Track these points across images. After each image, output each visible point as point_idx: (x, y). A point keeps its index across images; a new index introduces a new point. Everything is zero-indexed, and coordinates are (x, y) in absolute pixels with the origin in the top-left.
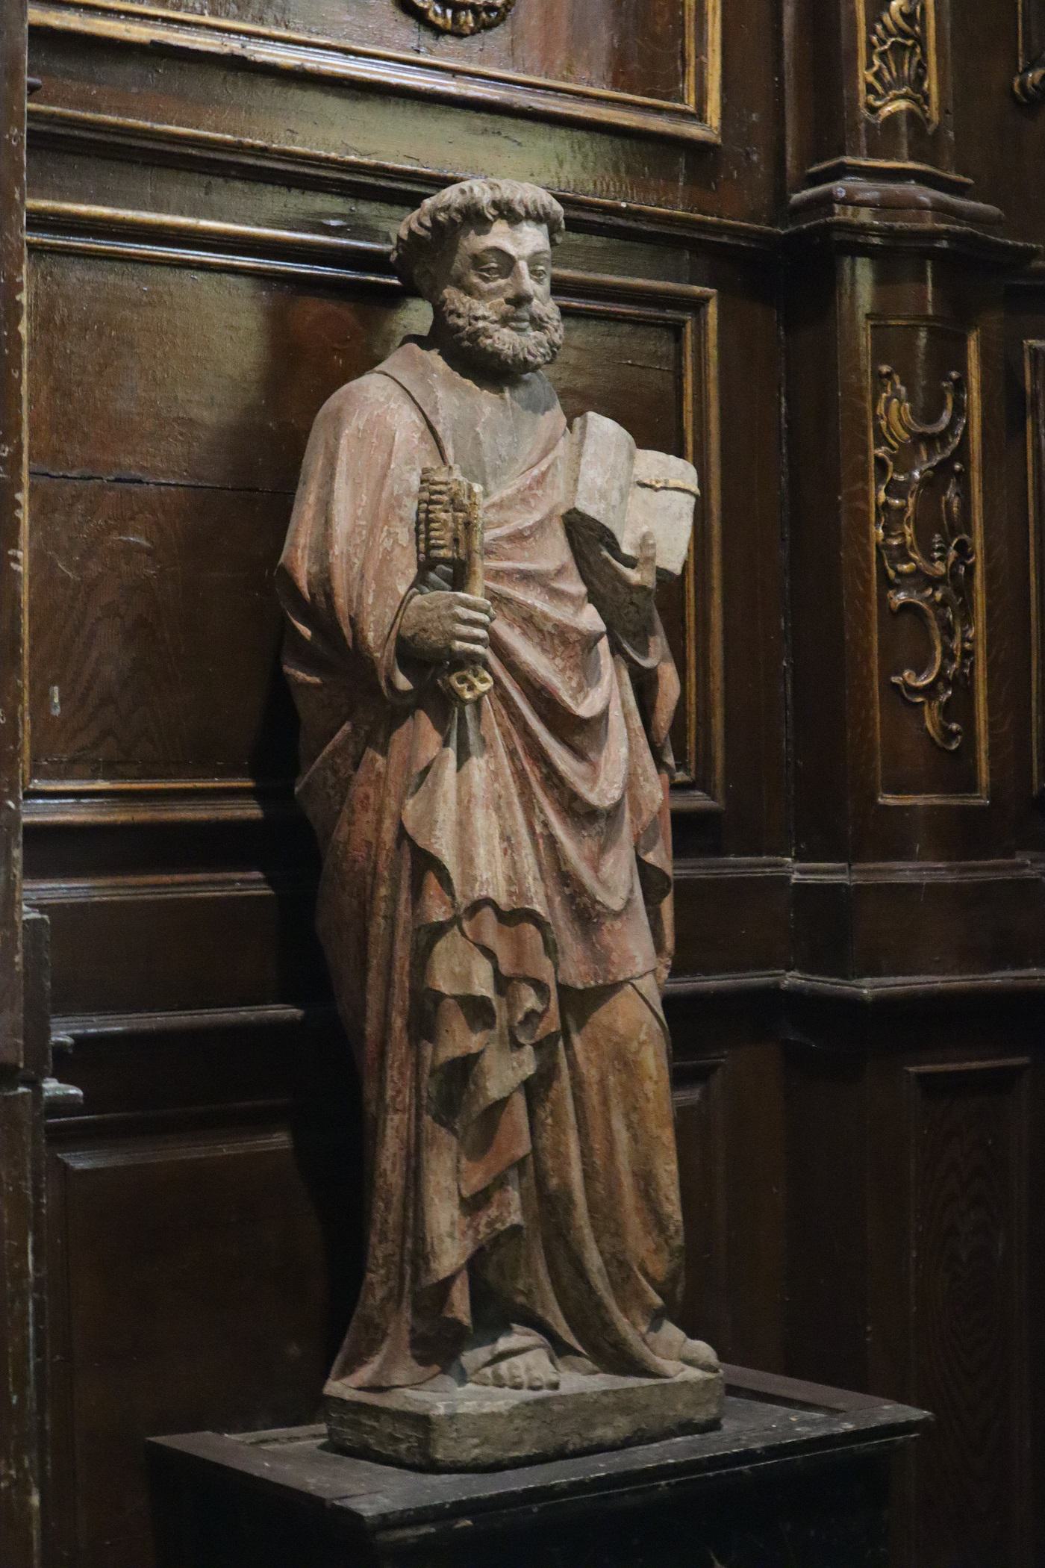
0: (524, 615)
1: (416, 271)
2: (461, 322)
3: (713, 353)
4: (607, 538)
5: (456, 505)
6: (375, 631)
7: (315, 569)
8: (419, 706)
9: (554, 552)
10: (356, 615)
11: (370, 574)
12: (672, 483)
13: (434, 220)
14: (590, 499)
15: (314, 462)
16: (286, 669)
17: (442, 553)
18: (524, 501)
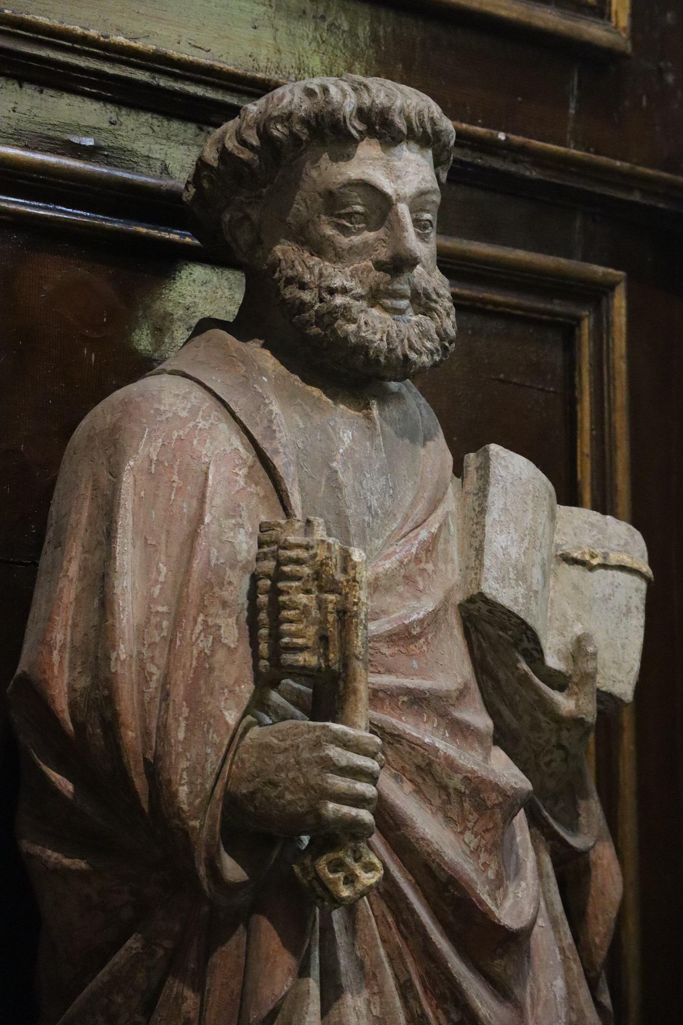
0: (419, 760)
1: (227, 217)
2: (307, 296)
3: (621, 366)
4: (523, 638)
5: (322, 581)
6: (191, 783)
7: (83, 682)
8: (257, 907)
9: (449, 667)
10: (157, 757)
11: (179, 692)
12: (613, 559)
13: (264, 135)
14: (502, 580)
15: (76, 513)
16: (26, 846)
17: (302, 658)
18: (408, 579)
